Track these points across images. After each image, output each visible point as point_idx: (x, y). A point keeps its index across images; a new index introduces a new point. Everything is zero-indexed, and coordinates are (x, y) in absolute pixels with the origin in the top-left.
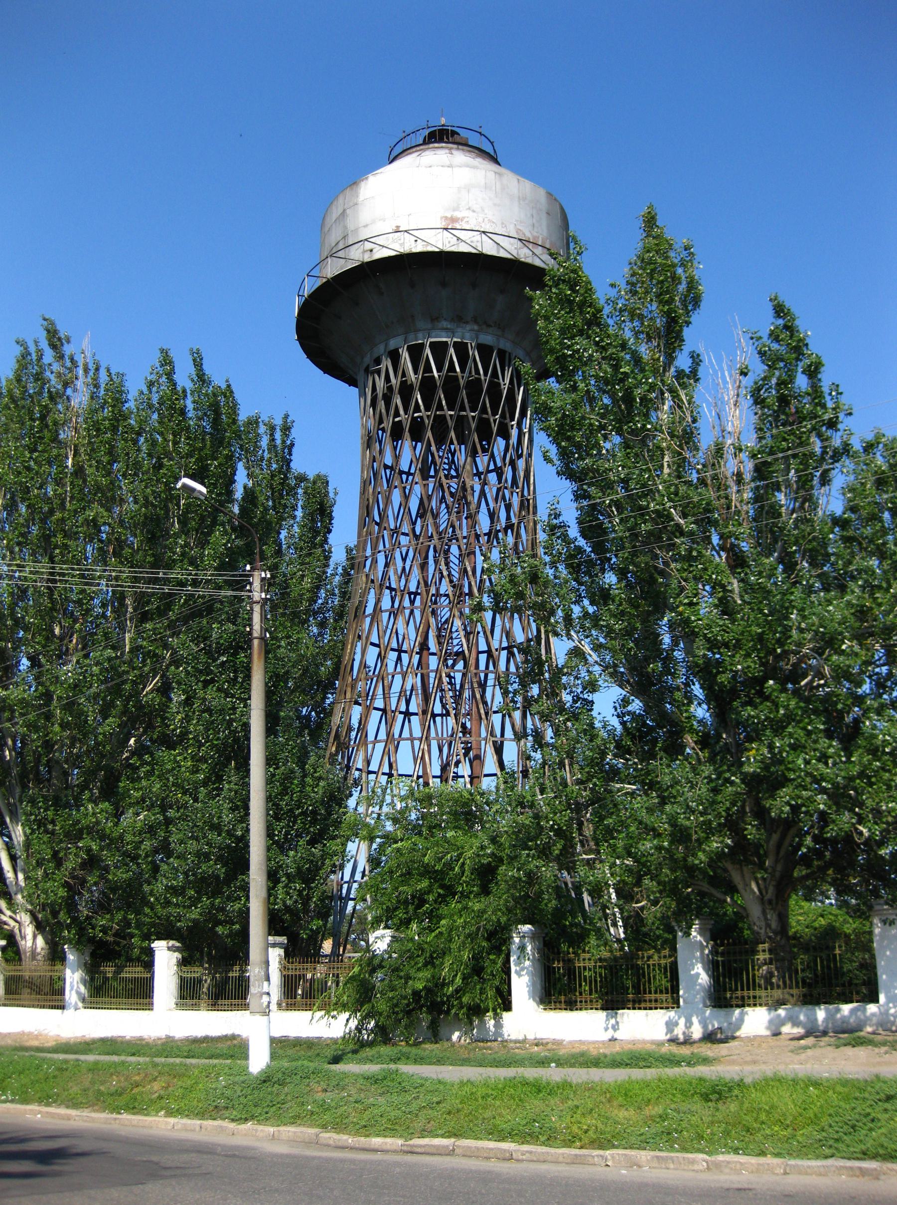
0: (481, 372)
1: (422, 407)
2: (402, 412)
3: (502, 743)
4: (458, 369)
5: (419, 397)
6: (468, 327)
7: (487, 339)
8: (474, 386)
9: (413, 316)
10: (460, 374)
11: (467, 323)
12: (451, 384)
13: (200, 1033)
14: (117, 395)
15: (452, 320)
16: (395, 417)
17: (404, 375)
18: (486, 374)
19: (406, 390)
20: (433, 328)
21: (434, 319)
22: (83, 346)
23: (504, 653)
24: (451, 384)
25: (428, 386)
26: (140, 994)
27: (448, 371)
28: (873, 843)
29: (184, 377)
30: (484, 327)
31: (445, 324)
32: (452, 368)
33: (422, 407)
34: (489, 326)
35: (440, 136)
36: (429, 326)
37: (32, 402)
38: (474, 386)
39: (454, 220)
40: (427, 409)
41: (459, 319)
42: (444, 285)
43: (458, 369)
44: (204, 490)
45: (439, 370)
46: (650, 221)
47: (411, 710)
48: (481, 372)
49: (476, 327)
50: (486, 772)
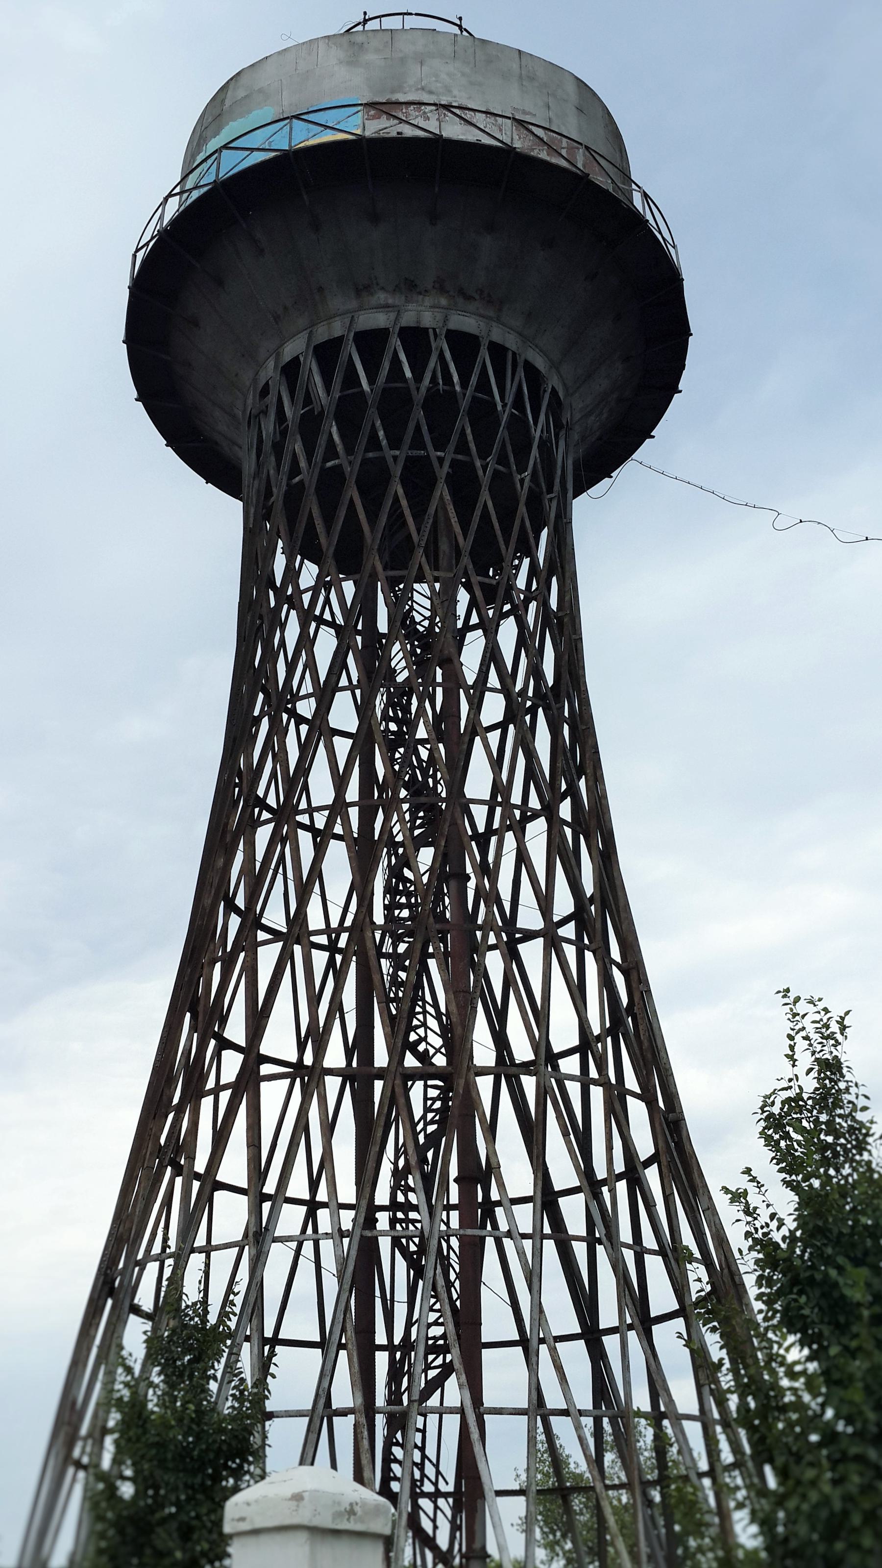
0: (456, 378)
1: (340, 448)
2: (303, 464)
3: (596, 1405)
4: (408, 374)
5: (334, 430)
6: (428, 301)
7: (466, 322)
8: (441, 404)
10: (412, 385)
12: (395, 403)
15: (397, 289)
16: (326, 460)
17: (308, 400)
18: (464, 384)
20: (361, 308)
21: (362, 289)
23: (622, 1187)
24: (395, 403)
25: (350, 411)
27: (389, 379)
30: (460, 300)
31: (382, 297)
33: (340, 448)
34: (469, 298)
36: (353, 304)
38: (441, 404)
41: (410, 287)
42: (375, 218)
43: (408, 374)
44: (242, 955)
45: (371, 381)
46: (847, 1013)
47: (222, 1176)
48: (456, 378)
49: (444, 302)
50: (351, 1418)
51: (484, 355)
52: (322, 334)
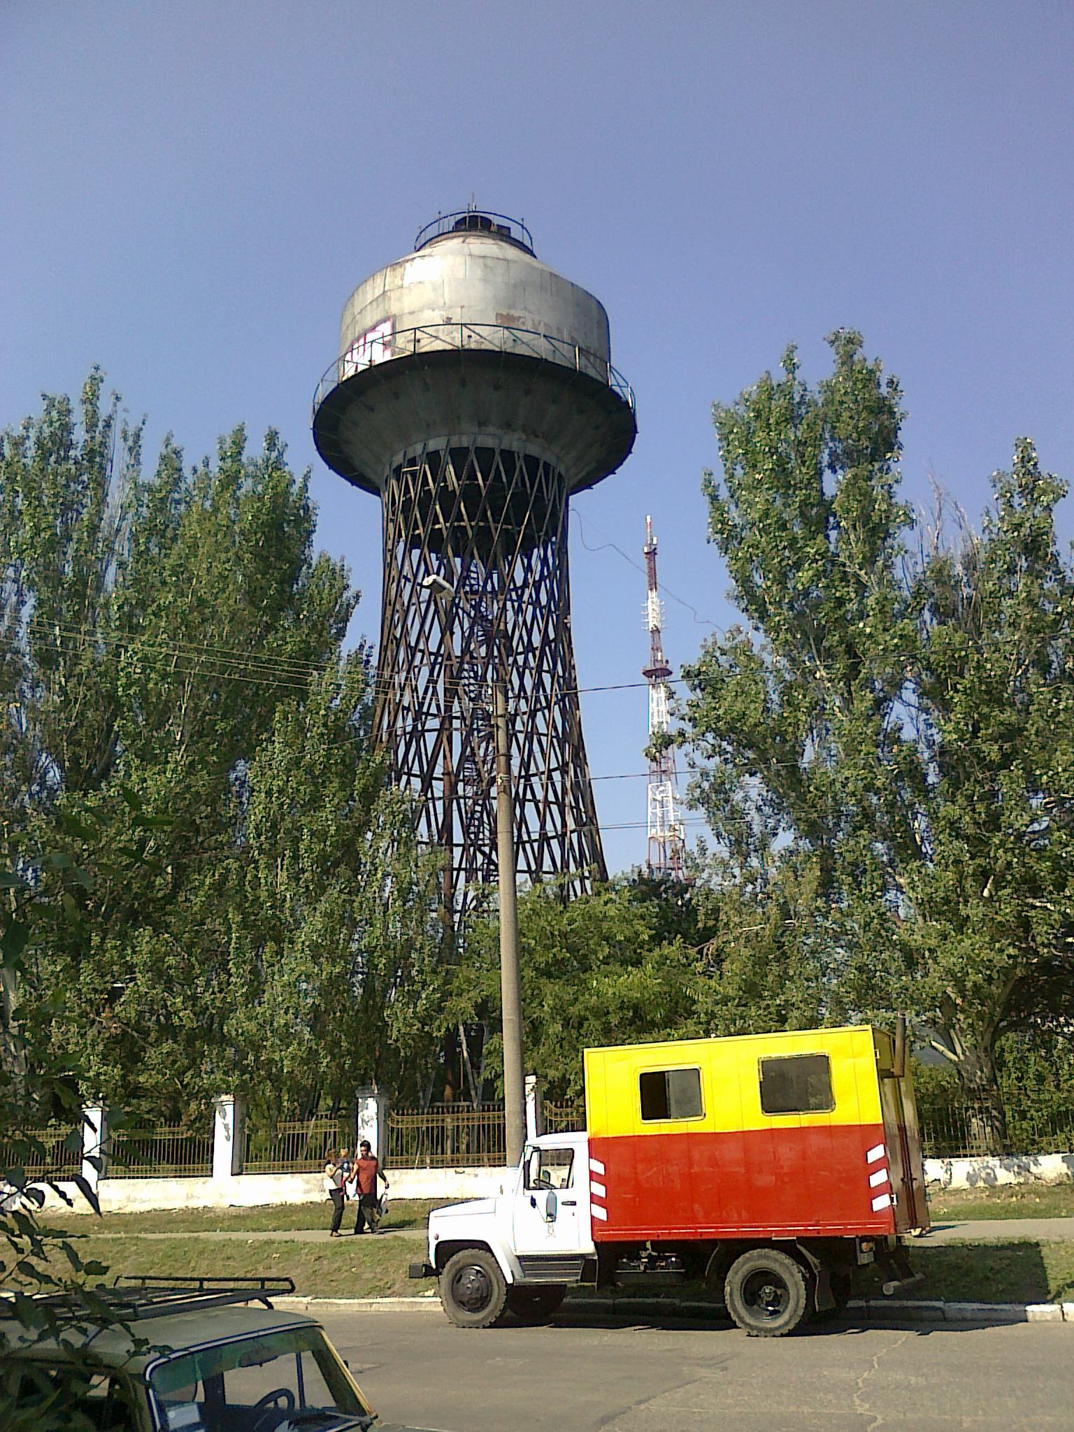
1: (465, 517)
4: (504, 479)
5: (438, 507)
6: (516, 436)
7: (534, 450)
9: (459, 418)
11: (514, 430)
13: (276, 1200)
14: (171, 461)
16: (434, 524)
17: (445, 481)
19: (446, 497)
21: (482, 424)
22: (727, 403)
26: (192, 1157)
28: (986, 1021)
29: (255, 450)
30: (532, 437)
32: (498, 476)
33: (465, 517)
34: (536, 436)
35: (474, 224)
36: (476, 429)
37: (67, 458)
39: (509, 318)
40: (470, 520)
41: (508, 426)
43: (504, 479)
49: (524, 437)
51: (498, 458)
52: (455, 443)
